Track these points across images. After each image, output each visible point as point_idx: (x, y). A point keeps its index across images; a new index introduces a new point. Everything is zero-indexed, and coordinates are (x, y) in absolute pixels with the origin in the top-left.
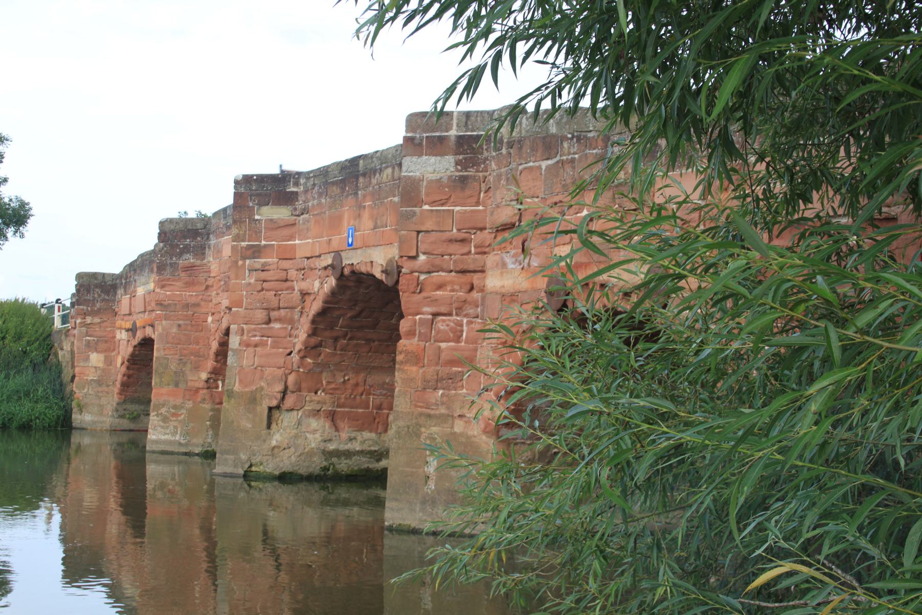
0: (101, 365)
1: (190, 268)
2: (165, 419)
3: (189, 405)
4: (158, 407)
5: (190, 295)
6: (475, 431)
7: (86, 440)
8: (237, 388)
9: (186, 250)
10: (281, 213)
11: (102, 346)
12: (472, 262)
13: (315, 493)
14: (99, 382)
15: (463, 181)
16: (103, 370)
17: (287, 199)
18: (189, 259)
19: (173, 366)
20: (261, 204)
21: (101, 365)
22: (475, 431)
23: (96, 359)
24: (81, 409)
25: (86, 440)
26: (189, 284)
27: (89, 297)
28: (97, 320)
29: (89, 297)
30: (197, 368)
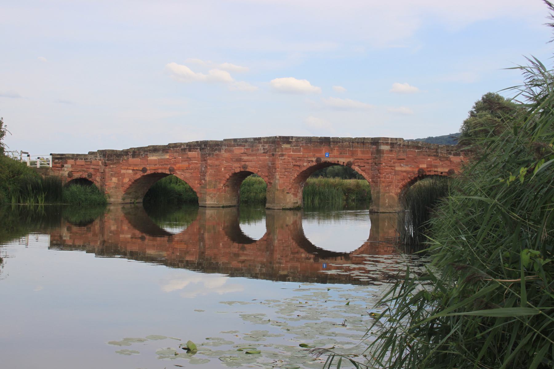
0: (116, 182)
1: (217, 155)
2: (212, 198)
3: (218, 193)
4: (209, 194)
5: (217, 163)
6: (393, 195)
7: (112, 208)
8: (279, 188)
9: (216, 150)
10: (288, 146)
11: (117, 175)
12: (393, 165)
13: (292, 212)
14: (116, 188)
15: (391, 151)
16: (117, 183)
17: (289, 143)
18: (217, 152)
19: (213, 183)
20: (284, 143)
21: (116, 182)
22: (393, 195)
23: (114, 180)
24: (109, 197)
25: (112, 208)
26: (217, 160)
27: (112, 158)
28: (115, 166)
29: (112, 158)
30: (220, 183)
